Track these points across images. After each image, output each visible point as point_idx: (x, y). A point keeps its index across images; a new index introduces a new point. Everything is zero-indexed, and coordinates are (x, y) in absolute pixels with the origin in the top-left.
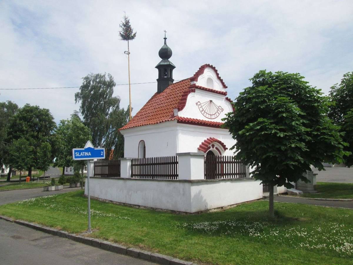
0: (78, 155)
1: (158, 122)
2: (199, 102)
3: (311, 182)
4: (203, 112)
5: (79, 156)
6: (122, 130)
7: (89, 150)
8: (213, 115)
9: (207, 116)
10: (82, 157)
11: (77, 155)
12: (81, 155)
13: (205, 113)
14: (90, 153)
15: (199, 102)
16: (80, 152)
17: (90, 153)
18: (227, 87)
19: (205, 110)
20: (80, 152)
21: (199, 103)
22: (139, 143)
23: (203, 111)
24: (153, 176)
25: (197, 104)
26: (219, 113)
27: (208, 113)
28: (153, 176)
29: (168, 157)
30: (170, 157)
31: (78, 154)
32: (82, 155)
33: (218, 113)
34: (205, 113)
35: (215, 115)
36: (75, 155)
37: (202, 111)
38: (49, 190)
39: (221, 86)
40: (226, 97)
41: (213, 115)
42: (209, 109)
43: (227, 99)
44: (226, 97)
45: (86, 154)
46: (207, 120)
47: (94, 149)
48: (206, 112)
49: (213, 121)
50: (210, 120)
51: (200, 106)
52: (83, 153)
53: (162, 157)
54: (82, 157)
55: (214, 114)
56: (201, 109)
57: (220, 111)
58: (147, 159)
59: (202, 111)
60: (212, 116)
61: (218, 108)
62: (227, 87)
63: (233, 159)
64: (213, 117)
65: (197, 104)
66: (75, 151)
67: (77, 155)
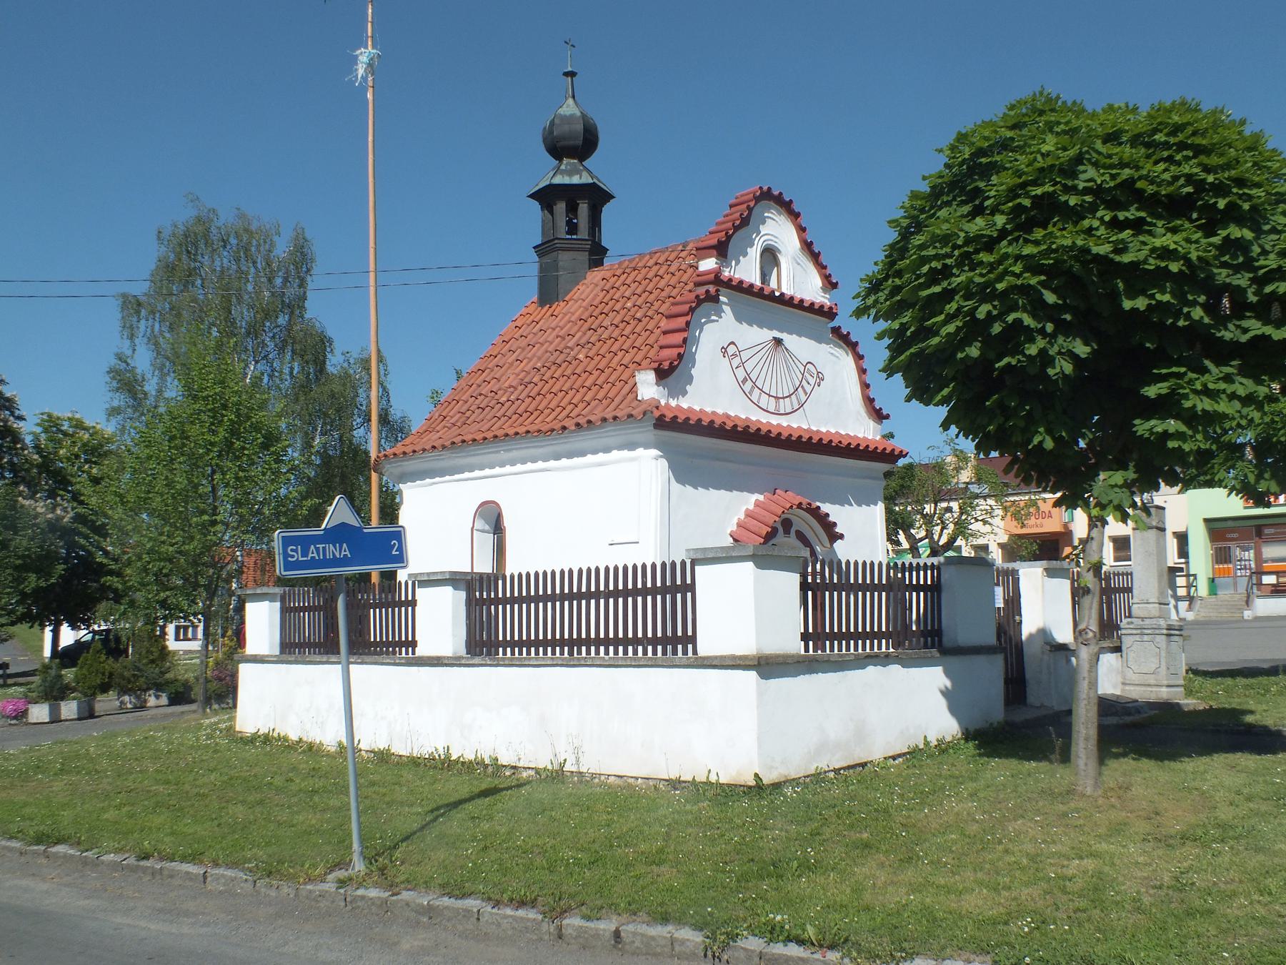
0: (298, 556)
1: (569, 423)
2: (733, 343)
3: (749, 424)
4: (749, 385)
5: (301, 559)
6: (426, 454)
7: (340, 533)
8: (783, 398)
9: (764, 401)
10: (313, 564)
11: (293, 557)
12: (310, 555)
13: (757, 391)
14: (345, 545)
15: (733, 343)
16: (305, 543)
17: (345, 545)
18: (887, 417)
19: (753, 377)
20: (305, 543)
21: (732, 349)
22: (479, 507)
23: (747, 383)
24: (574, 643)
25: (724, 350)
26: (808, 389)
27: (766, 389)
28: (574, 643)
29: (520, 575)
30: (545, 573)
31: (296, 551)
32: (315, 555)
33: (804, 391)
34: (757, 391)
35: (793, 397)
36: (286, 555)
37: (745, 381)
38: (63, 717)
39: (817, 281)
40: (835, 323)
41: (783, 398)
42: (774, 380)
43: (836, 331)
44: (835, 323)
45: (332, 550)
46: (764, 418)
47: (360, 529)
48: (759, 384)
49: (784, 421)
50: (775, 420)
51: (736, 362)
52: (317, 549)
53: (635, 567)
54: (313, 564)
55: (790, 396)
56: (741, 374)
57: (812, 381)
58: (512, 577)
59: (745, 381)
60: (781, 400)
61: (802, 369)
62: (887, 417)
63: (892, 571)
64: (785, 405)
65: (724, 350)
66: (287, 542)
67: (293, 557)
